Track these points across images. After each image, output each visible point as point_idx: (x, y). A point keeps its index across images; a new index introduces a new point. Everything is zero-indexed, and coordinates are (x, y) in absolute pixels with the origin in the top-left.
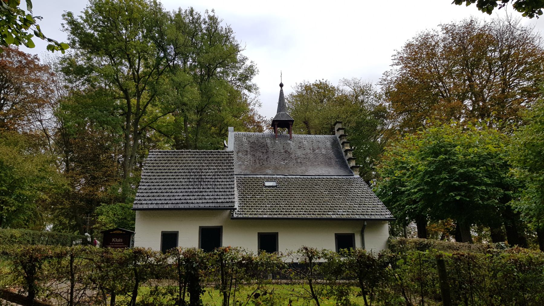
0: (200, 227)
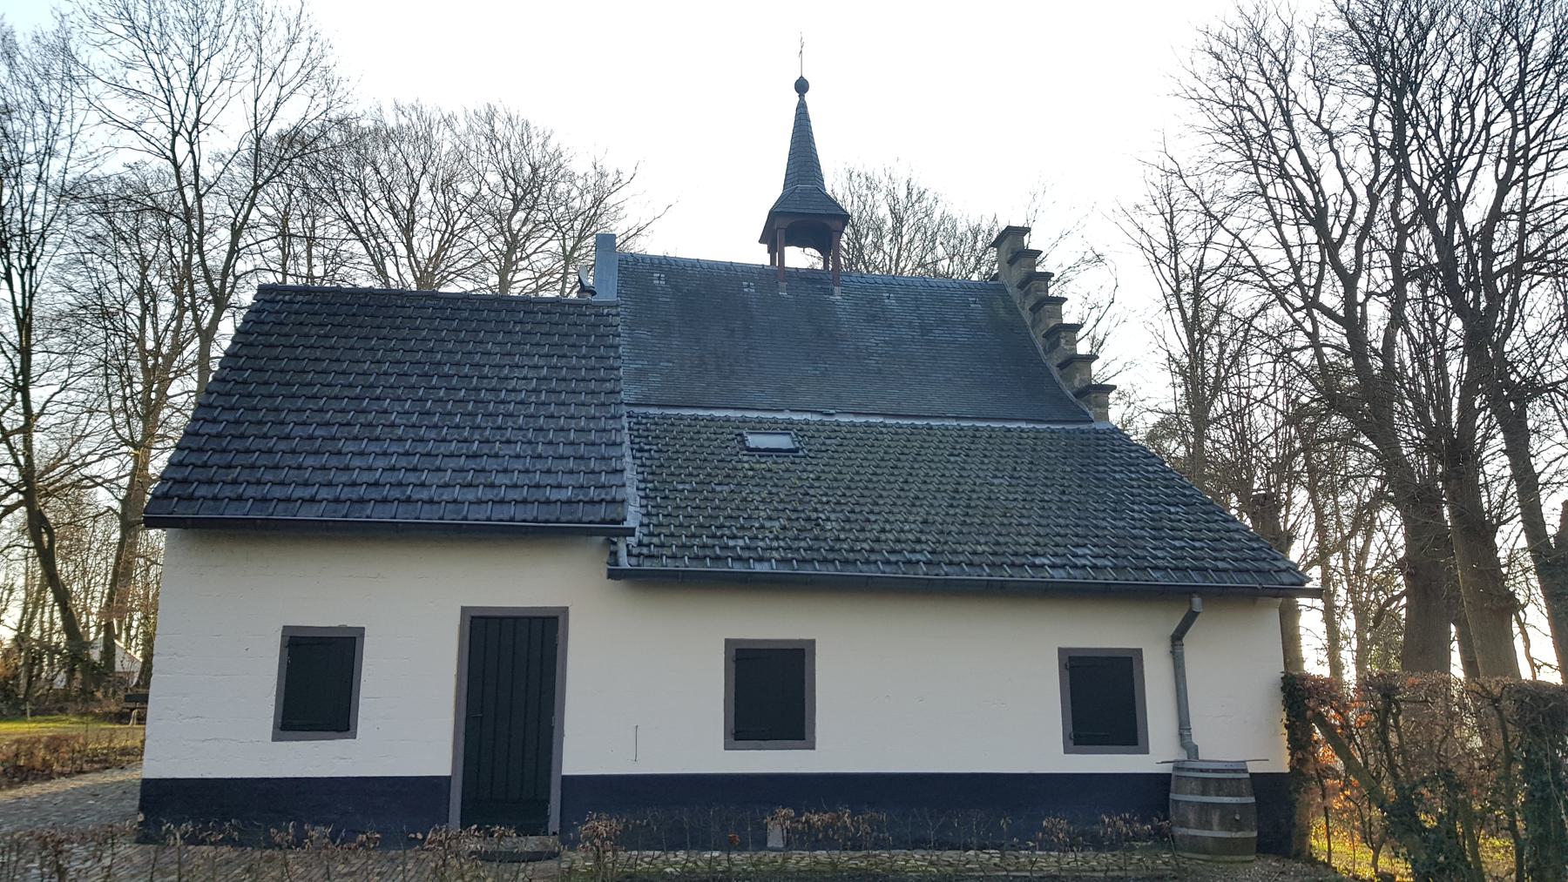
0: (729, 643)
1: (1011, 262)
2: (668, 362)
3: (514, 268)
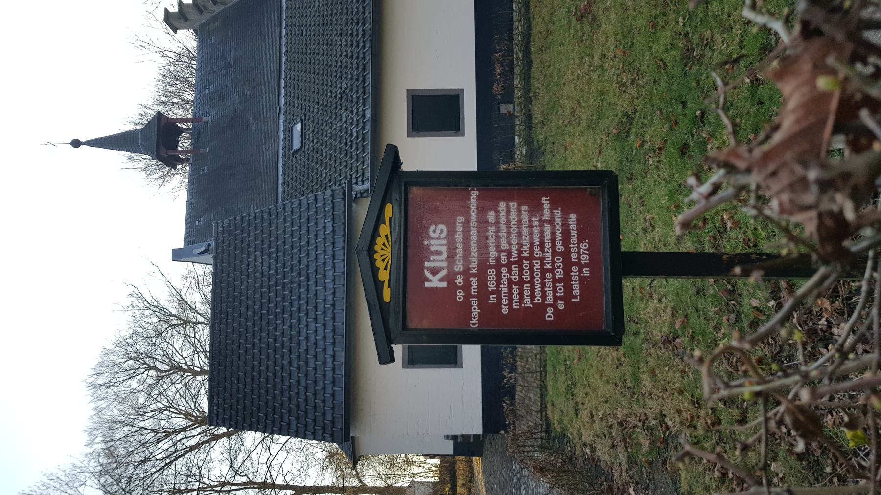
1: (186, 19)
2: (250, 207)
3: (192, 367)
